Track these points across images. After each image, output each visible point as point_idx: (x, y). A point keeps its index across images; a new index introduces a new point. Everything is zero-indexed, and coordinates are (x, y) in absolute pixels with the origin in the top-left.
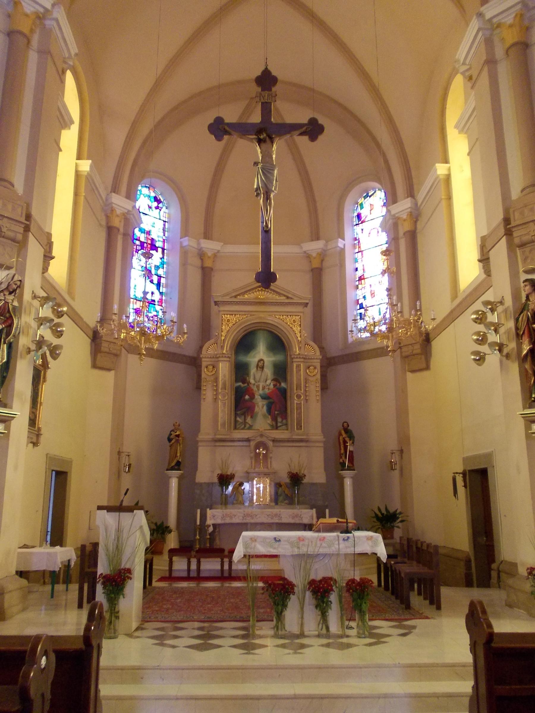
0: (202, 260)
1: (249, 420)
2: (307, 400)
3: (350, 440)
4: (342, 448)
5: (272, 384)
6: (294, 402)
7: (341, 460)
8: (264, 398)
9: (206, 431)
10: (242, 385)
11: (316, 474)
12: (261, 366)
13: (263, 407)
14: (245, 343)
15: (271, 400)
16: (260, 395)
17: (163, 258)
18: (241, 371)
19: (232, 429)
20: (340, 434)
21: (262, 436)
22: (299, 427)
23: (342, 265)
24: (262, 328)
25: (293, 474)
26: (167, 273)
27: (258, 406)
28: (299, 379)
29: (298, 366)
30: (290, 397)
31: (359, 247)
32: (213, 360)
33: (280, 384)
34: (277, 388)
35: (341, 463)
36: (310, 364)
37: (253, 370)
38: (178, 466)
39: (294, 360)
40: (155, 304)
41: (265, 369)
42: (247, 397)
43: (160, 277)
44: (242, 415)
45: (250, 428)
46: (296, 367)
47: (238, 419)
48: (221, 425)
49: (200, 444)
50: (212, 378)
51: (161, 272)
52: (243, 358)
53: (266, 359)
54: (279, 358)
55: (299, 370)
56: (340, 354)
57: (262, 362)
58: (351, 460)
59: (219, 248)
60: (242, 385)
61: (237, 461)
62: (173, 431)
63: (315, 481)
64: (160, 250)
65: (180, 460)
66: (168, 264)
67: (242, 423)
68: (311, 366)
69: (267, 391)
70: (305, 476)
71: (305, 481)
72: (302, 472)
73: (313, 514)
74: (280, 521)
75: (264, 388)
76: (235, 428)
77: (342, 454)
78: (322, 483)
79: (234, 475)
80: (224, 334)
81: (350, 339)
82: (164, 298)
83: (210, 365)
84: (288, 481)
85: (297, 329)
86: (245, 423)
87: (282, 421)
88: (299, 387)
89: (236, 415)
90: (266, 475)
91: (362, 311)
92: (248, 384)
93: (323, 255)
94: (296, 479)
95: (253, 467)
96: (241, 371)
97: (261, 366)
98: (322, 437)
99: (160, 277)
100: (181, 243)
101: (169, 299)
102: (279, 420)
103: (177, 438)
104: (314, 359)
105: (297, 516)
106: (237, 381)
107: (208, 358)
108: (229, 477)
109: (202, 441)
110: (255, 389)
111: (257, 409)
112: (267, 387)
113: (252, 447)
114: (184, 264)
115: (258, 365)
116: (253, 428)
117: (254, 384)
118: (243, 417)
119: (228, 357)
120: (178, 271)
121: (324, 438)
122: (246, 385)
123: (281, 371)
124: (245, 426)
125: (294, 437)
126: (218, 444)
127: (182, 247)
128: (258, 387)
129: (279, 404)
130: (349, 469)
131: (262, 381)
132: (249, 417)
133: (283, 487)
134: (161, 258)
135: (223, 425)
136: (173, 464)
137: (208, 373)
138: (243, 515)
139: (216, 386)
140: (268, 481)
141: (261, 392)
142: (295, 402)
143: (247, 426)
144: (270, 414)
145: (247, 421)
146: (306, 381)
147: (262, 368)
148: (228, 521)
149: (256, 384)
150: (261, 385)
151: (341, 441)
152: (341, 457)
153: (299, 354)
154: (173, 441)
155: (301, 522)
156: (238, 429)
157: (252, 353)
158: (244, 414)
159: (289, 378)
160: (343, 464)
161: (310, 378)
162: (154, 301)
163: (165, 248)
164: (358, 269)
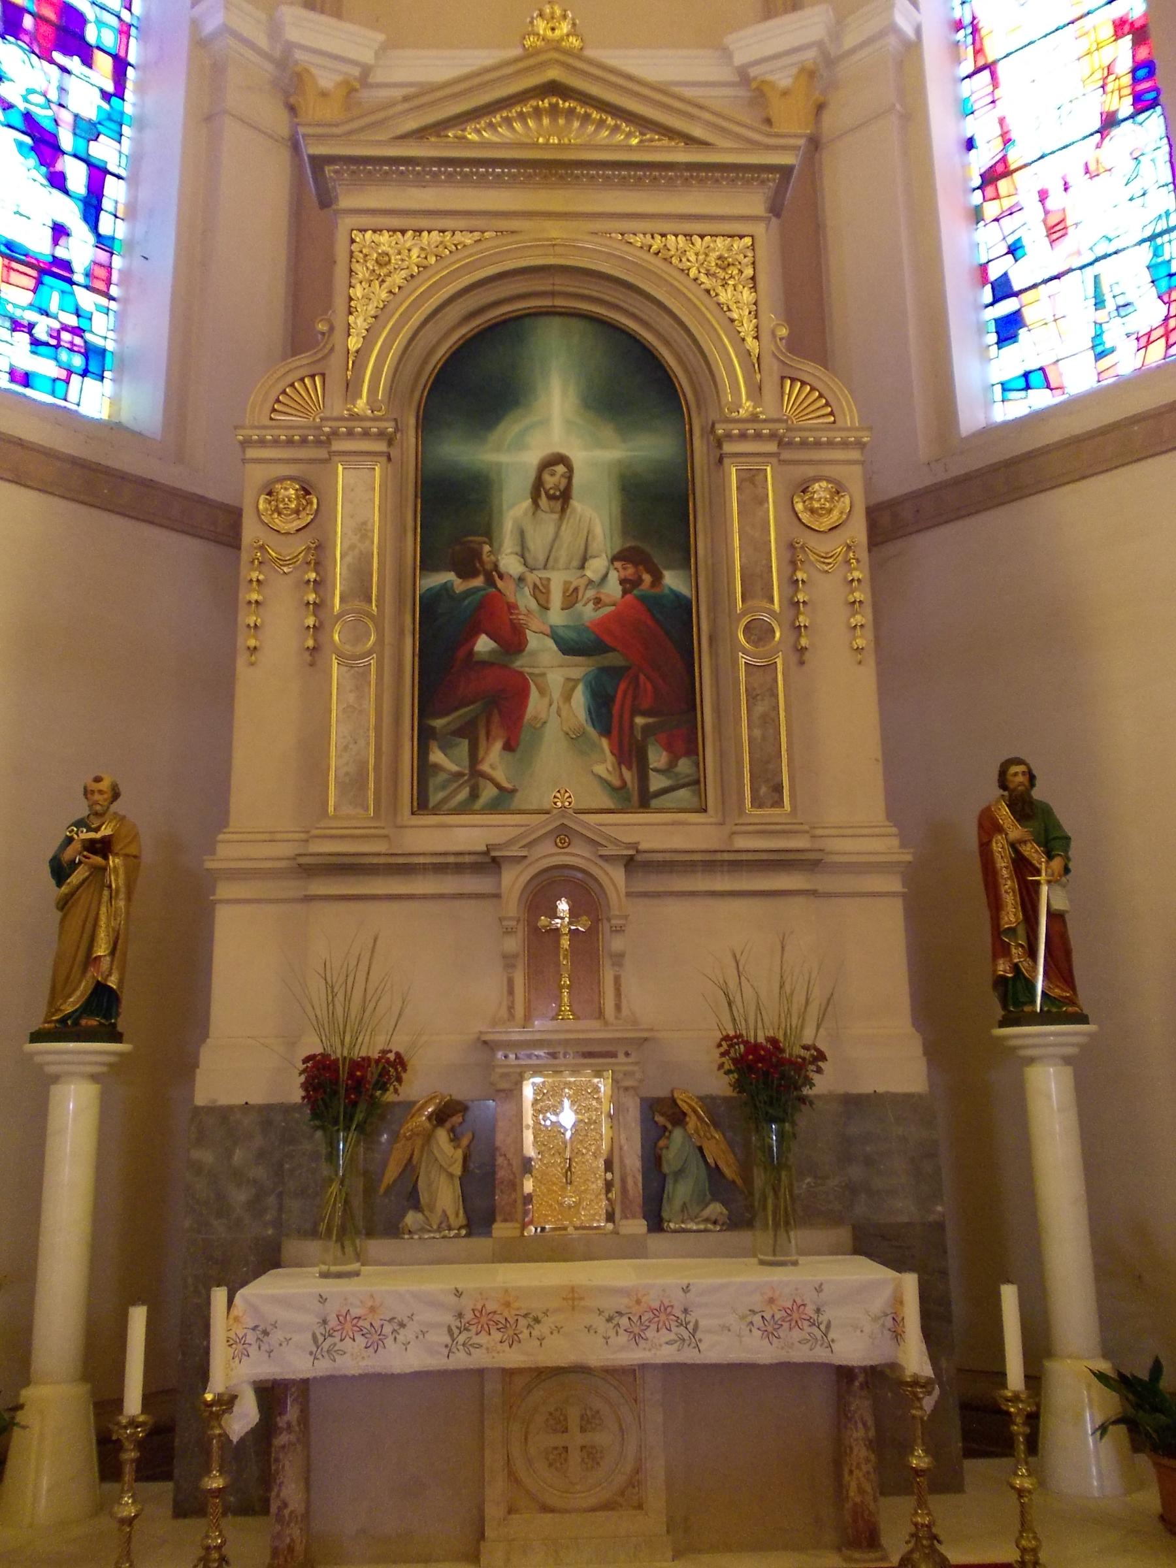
0: (292, 109)
1: (494, 760)
2: (803, 650)
3: (1050, 857)
4: (1010, 900)
5: (614, 577)
6: (728, 664)
7: (1003, 968)
8: (569, 648)
9: (262, 812)
10: (460, 586)
11: (876, 1052)
12: (553, 489)
13: (568, 697)
14: (470, 377)
15: (614, 659)
16: (554, 635)
17: (120, 92)
18: (449, 513)
19: (407, 810)
20: (988, 826)
21: (563, 835)
22: (769, 790)
23: (911, 114)
24: (559, 302)
25: (753, 1048)
26: (135, 160)
27: (542, 692)
28: (756, 546)
29: (750, 479)
30: (711, 639)
31: (978, 51)
32: (303, 453)
33: (657, 578)
34: (643, 599)
35: (1000, 983)
36: (810, 471)
37: (514, 510)
38: (98, 1014)
39: (728, 448)
40: (71, 282)
41: (577, 504)
42: (484, 644)
43: (98, 174)
44: (460, 732)
45: (504, 800)
46: (740, 482)
47: (437, 756)
48: (339, 784)
49: (224, 890)
50: (298, 546)
51: (103, 150)
52: (461, 452)
53: (579, 456)
54: (648, 448)
55: (754, 500)
56: (928, 481)
57: (560, 469)
58: (1061, 966)
59: (366, 56)
60: (460, 586)
61: (433, 990)
62: (80, 824)
63: (866, 1087)
64: (103, 63)
65: (112, 983)
66: (140, 123)
67: (459, 775)
68: (818, 479)
69: (588, 613)
70: (821, 1056)
71: (823, 1084)
72: (808, 1037)
73: (898, 1300)
74: (689, 1356)
75: (571, 598)
76: (422, 805)
77: (1012, 931)
78: (908, 1096)
79: (400, 1062)
80: (359, 323)
81: (970, 419)
82: (117, 263)
83: (281, 480)
84: (720, 1085)
85: (738, 298)
86: (475, 774)
87: (672, 764)
88: (756, 584)
89: (425, 736)
90: (594, 1054)
91: (1007, 307)
92: (490, 582)
93: (820, 78)
94: (767, 1076)
95: (519, 1011)
96: (449, 513)
97: (553, 489)
98: (895, 842)
99: (98, 174)
100: (195, 24)
101: (138, 262)
102: (657, 757)
103: (98, 860)
104: (830, 444)
105: (794, 1315)
106: (429, 562)
107: (276, 442)
108: (372, 1074)
109: (234, 875)
110: (525, 601)
111: (535, 704)
112: (590, 593)
113: (512, 906)
114: (207, 117)
115: (538, 485)
116: (517, 802)
117: (521, 579)
118: (464, 744)
119: (381, 434)
120: (180, 137)
121: (903, 845)
122: (478, 582)
123: (661, 514)
124: (474, 795)
125: (741, 843)
126: (320, 887)
127: (200, 43)
128: (541, 593)
129: (653, 678)
130: (1062, 1010)
131: (560, 561)
132: (498, 745)
133: (692, 1122)
134: (106, 96)
135: (355, 784)
136: (71, 1005)
137: (278, 522)
138: (449, 1319)
139: (318, 565)
140: (604, 1086)
141: (557, 617)
142: (743, 659)
143: (488, 792)
144: (606, 732)
145: (485, 767)
146: (794, 554)
147: (564, 497)
148: (354, 1359)
149: (531, 578)
150: (557, 581)
151: (1003, 864)
152: (1001, 950)
153: (754, 418)
154: (75, 879)
155: (820, 1355)
156: (435, 811)
157: (510, 428)
158: (467, 731)
159: (702, 546)
160: (1013, 995)
161: (812, 541)
162: (66, 265)
163: (131, 59)
164: (978, 142)
